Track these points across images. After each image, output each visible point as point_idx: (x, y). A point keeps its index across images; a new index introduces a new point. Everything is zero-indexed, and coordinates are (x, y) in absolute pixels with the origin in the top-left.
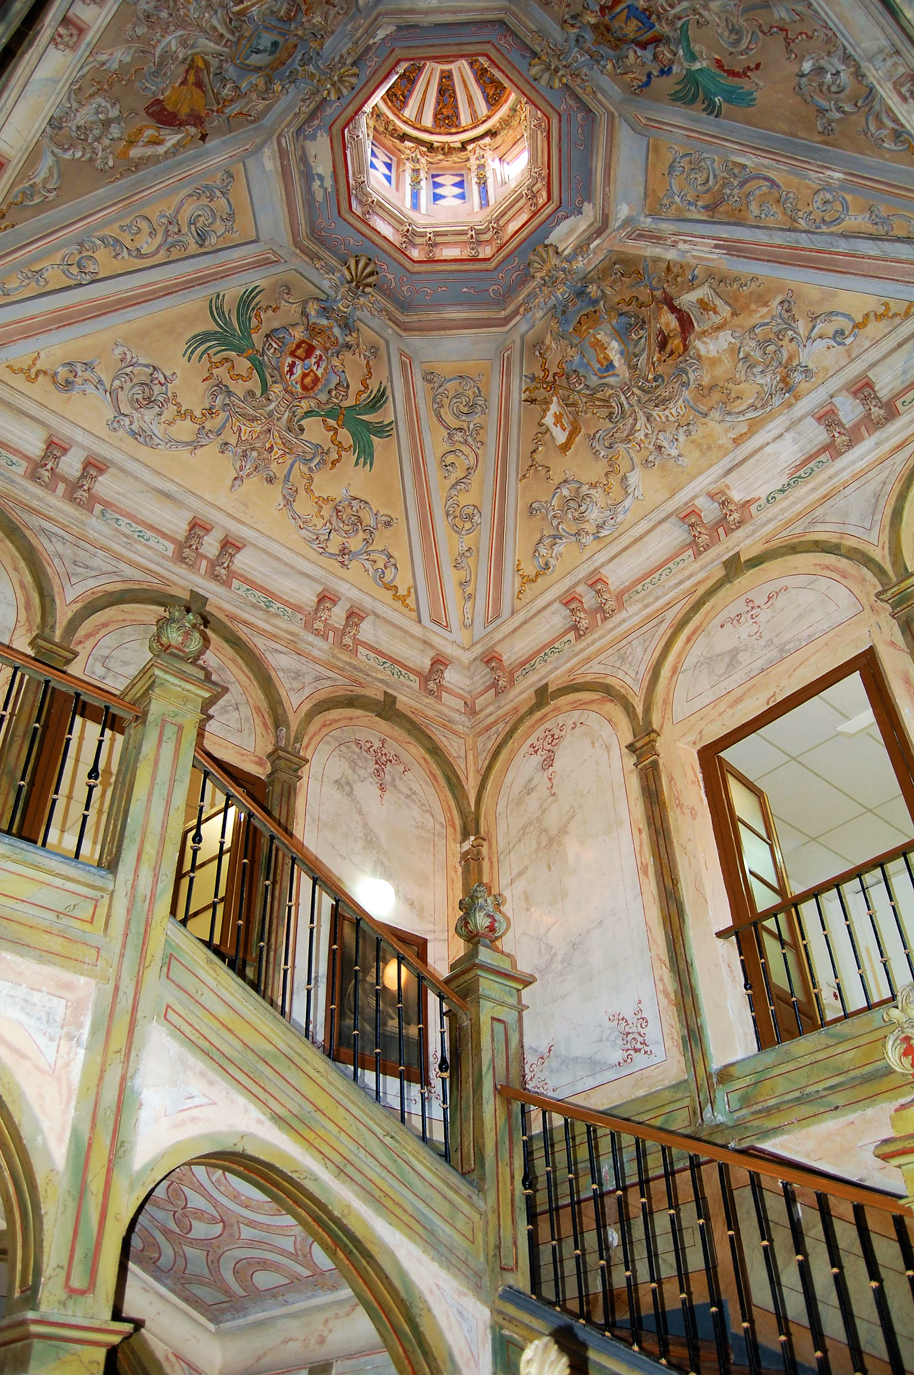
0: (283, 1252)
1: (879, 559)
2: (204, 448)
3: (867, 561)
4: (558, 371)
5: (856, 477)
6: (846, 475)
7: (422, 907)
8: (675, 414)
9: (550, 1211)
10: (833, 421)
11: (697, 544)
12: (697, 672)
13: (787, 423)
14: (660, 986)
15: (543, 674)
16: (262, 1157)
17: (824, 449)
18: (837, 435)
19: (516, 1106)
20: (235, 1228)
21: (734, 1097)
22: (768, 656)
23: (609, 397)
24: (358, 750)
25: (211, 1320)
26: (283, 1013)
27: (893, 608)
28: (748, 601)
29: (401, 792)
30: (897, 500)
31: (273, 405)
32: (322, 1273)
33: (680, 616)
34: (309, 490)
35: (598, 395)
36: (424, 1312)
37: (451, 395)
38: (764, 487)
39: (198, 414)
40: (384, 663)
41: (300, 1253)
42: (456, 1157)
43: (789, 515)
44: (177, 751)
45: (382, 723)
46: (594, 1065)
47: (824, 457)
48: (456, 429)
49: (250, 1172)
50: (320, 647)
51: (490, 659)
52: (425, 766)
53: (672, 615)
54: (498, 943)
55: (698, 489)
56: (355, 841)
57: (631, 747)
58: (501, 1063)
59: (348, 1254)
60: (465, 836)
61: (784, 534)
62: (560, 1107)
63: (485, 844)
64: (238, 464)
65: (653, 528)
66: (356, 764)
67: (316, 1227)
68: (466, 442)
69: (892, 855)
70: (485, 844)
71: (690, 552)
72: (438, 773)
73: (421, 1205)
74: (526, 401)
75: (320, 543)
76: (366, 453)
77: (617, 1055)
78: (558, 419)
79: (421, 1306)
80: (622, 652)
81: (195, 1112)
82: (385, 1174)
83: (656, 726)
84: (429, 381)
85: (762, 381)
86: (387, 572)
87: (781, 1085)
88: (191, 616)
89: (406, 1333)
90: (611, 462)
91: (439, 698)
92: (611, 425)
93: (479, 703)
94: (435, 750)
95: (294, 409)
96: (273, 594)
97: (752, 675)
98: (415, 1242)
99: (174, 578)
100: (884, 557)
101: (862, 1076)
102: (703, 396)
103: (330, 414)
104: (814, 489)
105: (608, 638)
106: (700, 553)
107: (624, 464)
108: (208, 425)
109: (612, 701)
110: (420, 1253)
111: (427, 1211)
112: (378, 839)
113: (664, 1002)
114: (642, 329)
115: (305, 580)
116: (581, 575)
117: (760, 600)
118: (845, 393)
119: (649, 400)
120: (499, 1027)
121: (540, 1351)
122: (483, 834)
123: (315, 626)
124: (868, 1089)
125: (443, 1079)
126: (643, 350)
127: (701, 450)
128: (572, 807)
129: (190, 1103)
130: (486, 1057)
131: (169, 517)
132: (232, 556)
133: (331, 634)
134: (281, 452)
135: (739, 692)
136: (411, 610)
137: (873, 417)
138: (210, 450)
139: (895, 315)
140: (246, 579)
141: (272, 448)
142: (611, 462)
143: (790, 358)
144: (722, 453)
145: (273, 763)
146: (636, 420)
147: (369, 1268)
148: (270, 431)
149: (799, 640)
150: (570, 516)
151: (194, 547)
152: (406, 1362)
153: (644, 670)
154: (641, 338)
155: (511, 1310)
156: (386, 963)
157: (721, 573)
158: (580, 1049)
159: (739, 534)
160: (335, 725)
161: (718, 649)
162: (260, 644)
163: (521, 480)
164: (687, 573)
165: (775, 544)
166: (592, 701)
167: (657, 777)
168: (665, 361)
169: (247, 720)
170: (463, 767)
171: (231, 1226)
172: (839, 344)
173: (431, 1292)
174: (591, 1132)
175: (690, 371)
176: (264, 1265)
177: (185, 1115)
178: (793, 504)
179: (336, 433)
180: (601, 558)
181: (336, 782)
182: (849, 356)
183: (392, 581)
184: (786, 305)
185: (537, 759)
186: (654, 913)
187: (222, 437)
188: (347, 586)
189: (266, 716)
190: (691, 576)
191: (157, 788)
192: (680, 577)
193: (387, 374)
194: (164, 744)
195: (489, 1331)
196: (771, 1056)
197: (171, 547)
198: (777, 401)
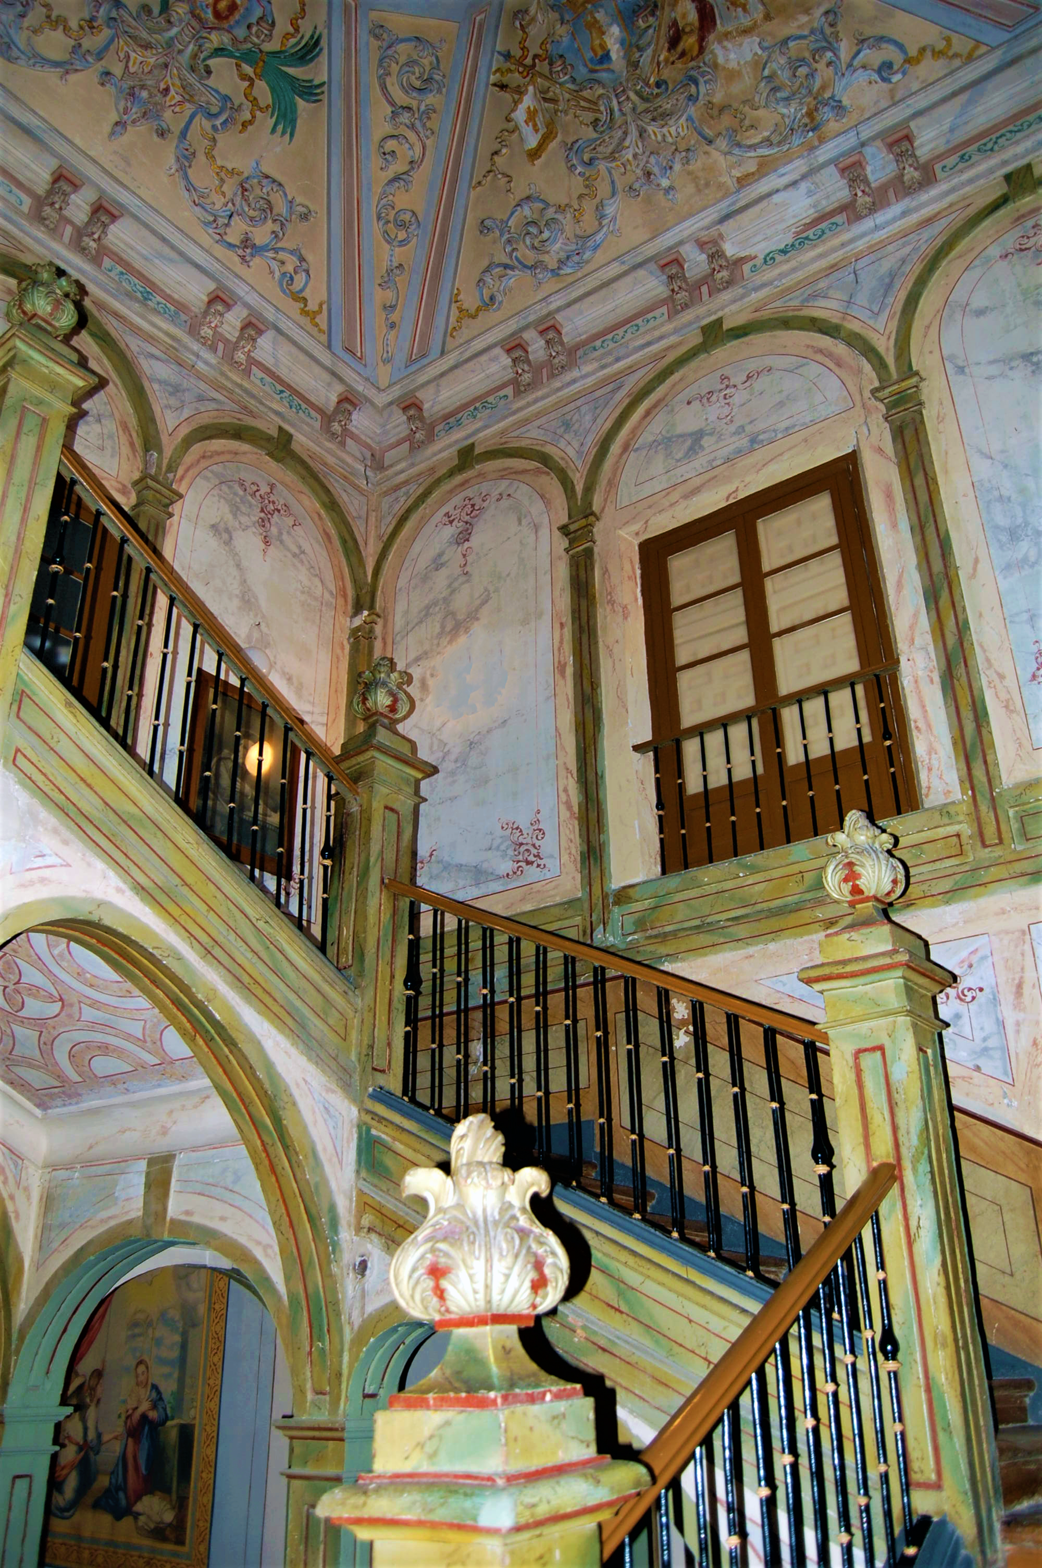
0: (128, 1037)
1: (882, 350)
2: (79, 74)
3: (869, 351)
4: (541, 52)
5: (872, 249)
6: (861, 245)
7: (301, 684)
8: (674, 134)
9: (433, 1017)
10: (858, 176)
11: (673, 300)
12: (652, 452)
13: (804, 169)
14: (563, 797)
15: (469, 431)
16: (121, 930)
17: (843, 209)
18: (860, 194)
19: (404, 904)
20: (76, 1008)
21: (629, 920)
22: (737, 444)
23: (599, 96)
24: (241, 493)
25: (38, 1106)
26: (151, 773)
27: (888, 409)
28: (723, 378)
29: (289, 550)
30: (915, 284)
31: (174, 31)
32: (172, 1062)
33: (641, 384)
34: (210, 156)
35: (586, 94)
36: (288, 1106)
37: (402, 60)
38: (763, 245)
39: (73, 24)
40: (282, 392)
41: (148, 1039)
42: (331, 950)
43: (787, 282)
44: (39, 448)
45: (273, 465)
46: (479, 874)
47: (839, 219)
48: (403, 108)
49: (105, 945)
50: (207, 361)
51: (411, 406)
52: (319, 523)
53: (632, 383)
54: (400, 727)
55: (686, 234)
56: (230, 599)
57: (564, 529)
58: (390, 856)
59: (209, 1041)
60: (358, 609)
61: (778, 304)
62: (461, 907)
63: (380, 621)
64: (122, 105)
65: (625, 274)
66: (238, 509)
67: (175, 1010)
68: (412, 127)
69: (837, 683)
70: (380, 621)
71: (664, 309)
72: (333, 532)
73: (292, 997)
74: (495, 85)
75: (217, 224)
76: (286, 119)
77: (506, 866)
78: (531, 115)
79: (286, 1099)
80: (567, 417)
81: (46, 873)
82: (255, 959)
83: (596, 508)
84: (377, 37)
85: (785, 111)
86: (296, 278)
87: (682, 912)
88: (63, 282)
89: (266, 1127)
90: (589, 183)
91: (343, 444)
92: (595, 135)
93: (389, 457)
94: (332, 505)
95: (201, 41)
96: (154, 284)
97: (714, 464)
98: (282, 1032)
99: (28, 241)
100: (888, 349)
101: (769, 910)
102: (712, 117)
103: (247, 57)
104: (821, 256)
105: (553, 399)
106: (677, 312)
107: (603, 188)
108: (86, 43)
109: (548, 474)
110: (289, 1045)
111: (298, 1003)
112: (257, 599)
113: (565, 814)
114: (653, 14)
115: (194, 271)
116: (532, 318)
117: (738, 379)
118: (878, 143)
119: (647, 111)
120: (392, 817)
121: (474, 1127)
122: (378, 610)
123: (202, 333)
124: (775, 923)
125: (325, 868)
126: (649, 44)
127: (697, 186)
128: (486, 590)
129: (40, 862)
130: (375, 848)
131: (27, 161)
132: (105, 226)
133: (221, 346)
134: (178, 98)
135: (697, 482)
136: (320, 331)
137: (906, 178)
138: (85, 79)
139: (956, 55)
140: (122, 259)
141: (167, 90)
142: (589, 183)
143: (823, 88)
144: (719, 195)
145: (139, 493)
146: (626, 133)
147: (231, 1057)
148: (166, 66)
149: (775, 431)
150: (528, 242)
151: (57, 206)
152: (264, 1155)
153: (591, 441)
154: (649, 27)
155: (381, 1110)
156: (246, 749)
157: (699, 339)
158: (466, 856)
159: (726, 296)
160: (217, 459)
161: (679, 430)
162: (133, 345)
163: (474, 188)
164: (657, 333)
165: (765, 314)
166: (524, 472)
167: (589, 567)
168: (673, 63)
169: (111, 437)
170: (363, 530)
171: (71, 1005)
172: (883, 79)
173: (298, 1085)
174: (488, 935)
175: (701, 80)
176: (105, 1049)
177: (34, 875)
178: (794, 270)
179: (252, 85)
180: (557, 302)
181: (213, 526)
182: (892, 98)
183: (301, 291)
184: (831, 18)
185: (449, 531)
186: (567, 718)
187: (103, 63)
188: (247, 289)
189: (134, 435)
190: (661, 338)
191: (12, 490)
192: (648, 338)
193: (325, 17)
194: (23, 437)
195: (355, 1130)
196: (674, 881)
197: (27, 201)
198: (796, 140)
